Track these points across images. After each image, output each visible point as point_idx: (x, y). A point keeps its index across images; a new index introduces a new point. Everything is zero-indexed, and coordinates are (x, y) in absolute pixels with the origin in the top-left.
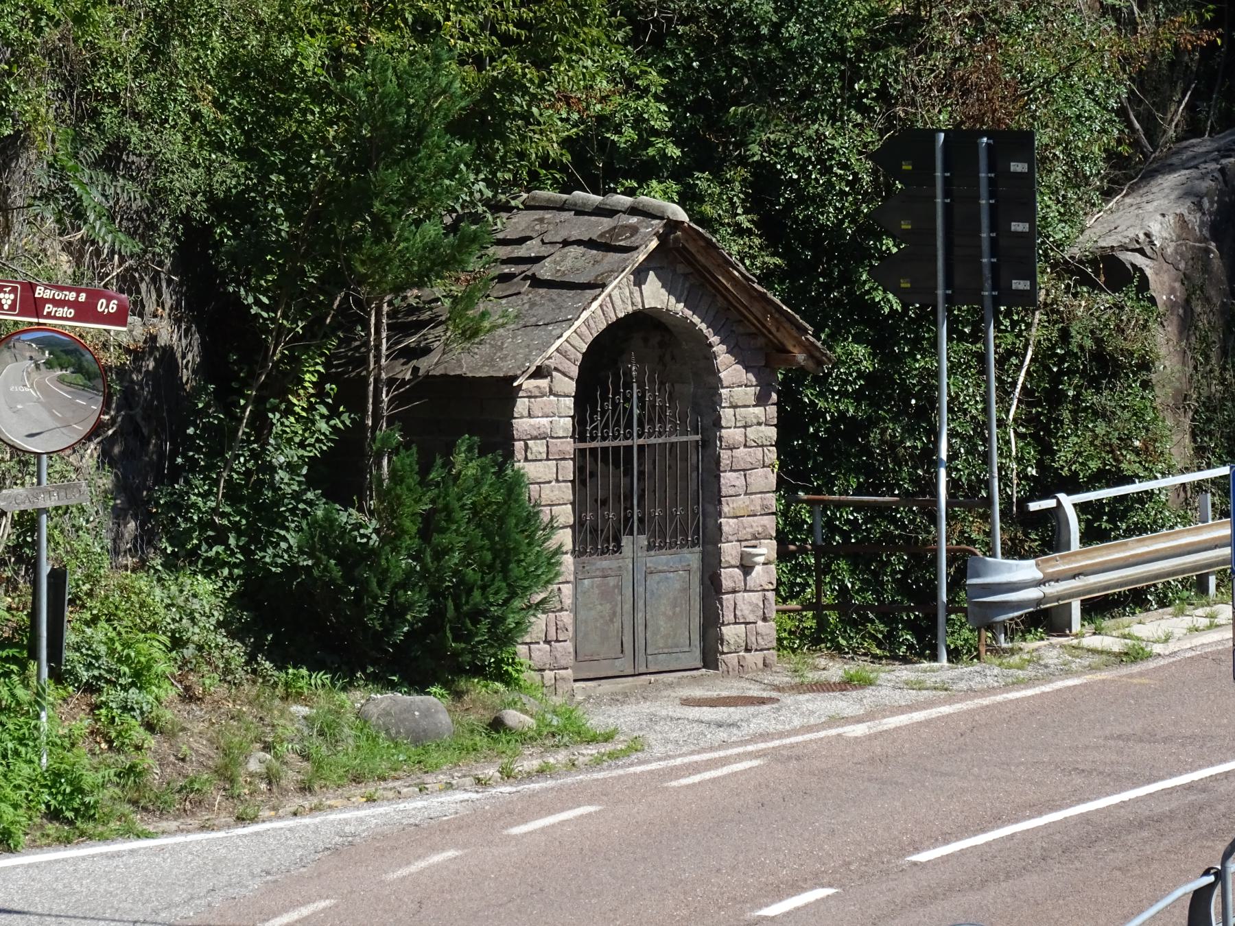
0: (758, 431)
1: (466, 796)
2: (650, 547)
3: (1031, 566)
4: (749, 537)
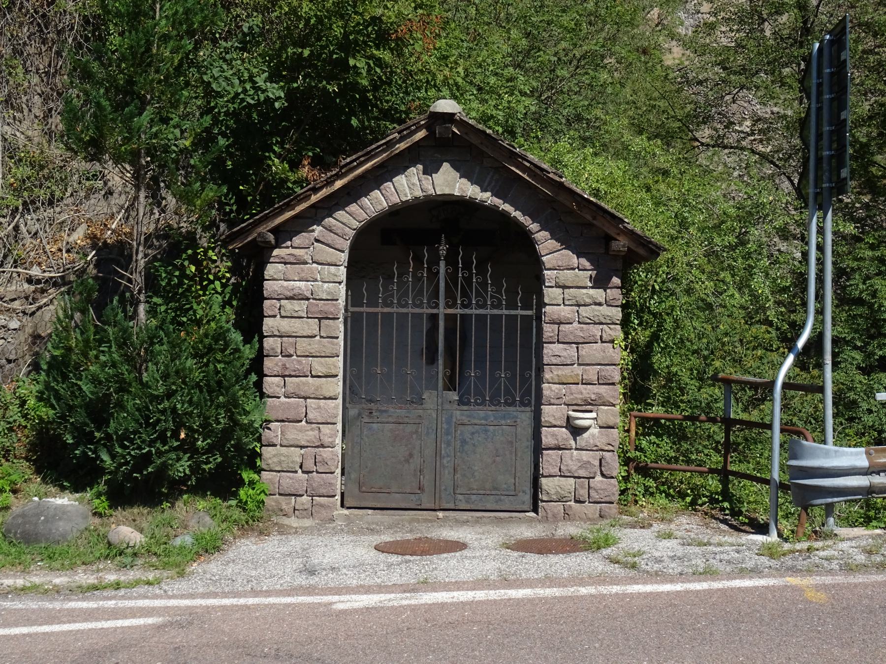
0: (594, 310)
1: (828, 580)
2: (461, 402)
3: (857, 454)
4: (580, 402)
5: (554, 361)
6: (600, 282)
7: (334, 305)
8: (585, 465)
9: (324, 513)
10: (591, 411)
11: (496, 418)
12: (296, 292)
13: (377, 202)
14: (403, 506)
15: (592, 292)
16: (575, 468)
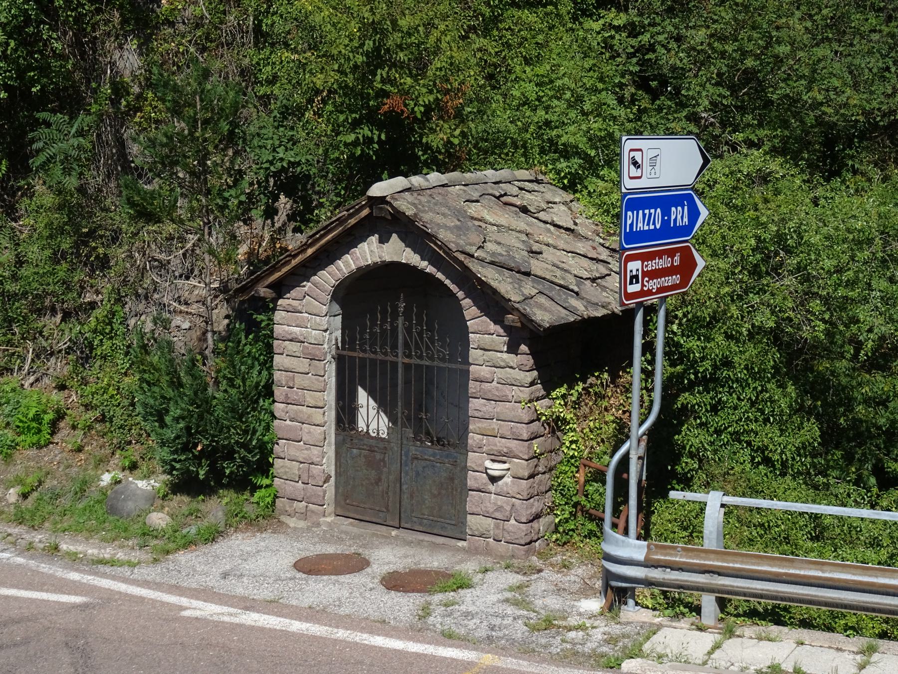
3: (640, 547)
4: (496, 453)
5: (477, 415)
6: (512, 349)
7: (320, 349)
8: (499, 509)
9: (314, 519)
10: (505, 462)
11: (441, 457)
12: (294, 336)
13: (348, 264)
14: (374, 520)
15: (505, 356)
16: (491, 510)
